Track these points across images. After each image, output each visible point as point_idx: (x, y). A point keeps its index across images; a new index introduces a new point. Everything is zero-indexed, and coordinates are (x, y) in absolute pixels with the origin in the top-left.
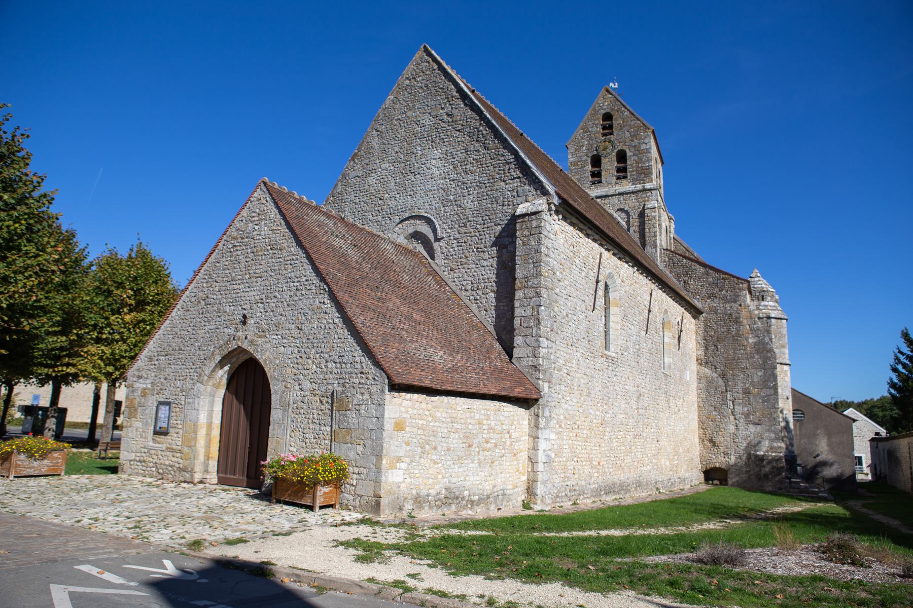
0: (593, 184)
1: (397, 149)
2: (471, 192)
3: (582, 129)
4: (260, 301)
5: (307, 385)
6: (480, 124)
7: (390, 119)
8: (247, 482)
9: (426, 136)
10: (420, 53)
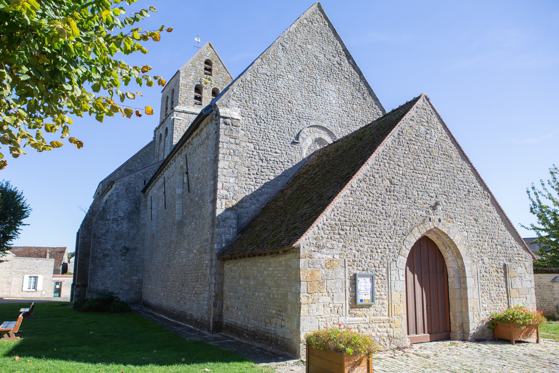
0: (196, 104)
1: (300, 68)
2: (357, 124)
3: (191, 63)
4: (443, 193)
5: (486, 260)
6: (360, 81)
7: (293, 43)
8: (430, 338)
9: (322, 70)
10: (315, 6)
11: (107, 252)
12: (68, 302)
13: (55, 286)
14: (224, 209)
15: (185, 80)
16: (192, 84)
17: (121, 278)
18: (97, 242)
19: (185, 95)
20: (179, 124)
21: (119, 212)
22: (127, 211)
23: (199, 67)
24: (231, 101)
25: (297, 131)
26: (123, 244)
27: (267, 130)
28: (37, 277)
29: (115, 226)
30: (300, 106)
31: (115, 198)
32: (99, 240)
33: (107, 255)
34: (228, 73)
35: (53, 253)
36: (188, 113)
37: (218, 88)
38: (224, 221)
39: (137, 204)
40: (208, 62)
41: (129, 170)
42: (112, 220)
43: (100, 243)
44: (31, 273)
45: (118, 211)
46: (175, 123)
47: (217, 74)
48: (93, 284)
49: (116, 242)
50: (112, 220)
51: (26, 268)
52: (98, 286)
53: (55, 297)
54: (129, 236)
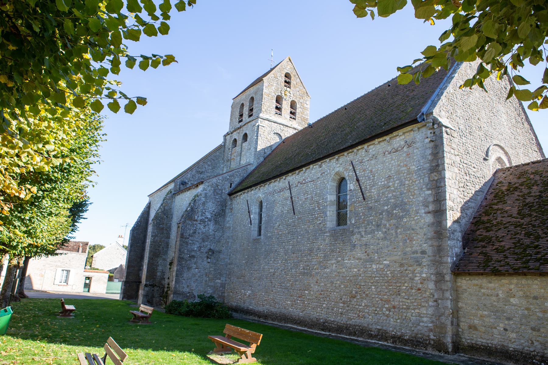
11: (193, 254)
12: (118, 300)
13: (86, 281)
14: (452, 221)
15: (267, 89)
16: (273, 94)
17: (206, 281)
18: (184, 242)
19: (268, 104)
20: (263, 131)
21: (207, 213)
22: (214, 213)
23: (280, 79)
24: (442, 111)
25: (486, 150)
26: (209, 246)
27: (467, 145)
28: (70, 271)
29: (202, 227)
30: (485, 124)
31: (203, 199)
32: (187, 240)
33: (193, 257)
34: (304, 88)
35: (75, 247)
36: (271, 121)
37: (296, 101)
38: (453, 233)
39: (223, 206)
40: (287, 76)
41: (200, 171)
42: (200, 221)
43: (187, 243)
44: (64, 266)
45: (205, 212)
46: (260, 130)
47: (295, 87)
48: (179, 286)
49: (203, 244)
50: (200, 221)
51: (59, 261)
52: (184, 287)
53: (84, 291)
54: (214, 238)
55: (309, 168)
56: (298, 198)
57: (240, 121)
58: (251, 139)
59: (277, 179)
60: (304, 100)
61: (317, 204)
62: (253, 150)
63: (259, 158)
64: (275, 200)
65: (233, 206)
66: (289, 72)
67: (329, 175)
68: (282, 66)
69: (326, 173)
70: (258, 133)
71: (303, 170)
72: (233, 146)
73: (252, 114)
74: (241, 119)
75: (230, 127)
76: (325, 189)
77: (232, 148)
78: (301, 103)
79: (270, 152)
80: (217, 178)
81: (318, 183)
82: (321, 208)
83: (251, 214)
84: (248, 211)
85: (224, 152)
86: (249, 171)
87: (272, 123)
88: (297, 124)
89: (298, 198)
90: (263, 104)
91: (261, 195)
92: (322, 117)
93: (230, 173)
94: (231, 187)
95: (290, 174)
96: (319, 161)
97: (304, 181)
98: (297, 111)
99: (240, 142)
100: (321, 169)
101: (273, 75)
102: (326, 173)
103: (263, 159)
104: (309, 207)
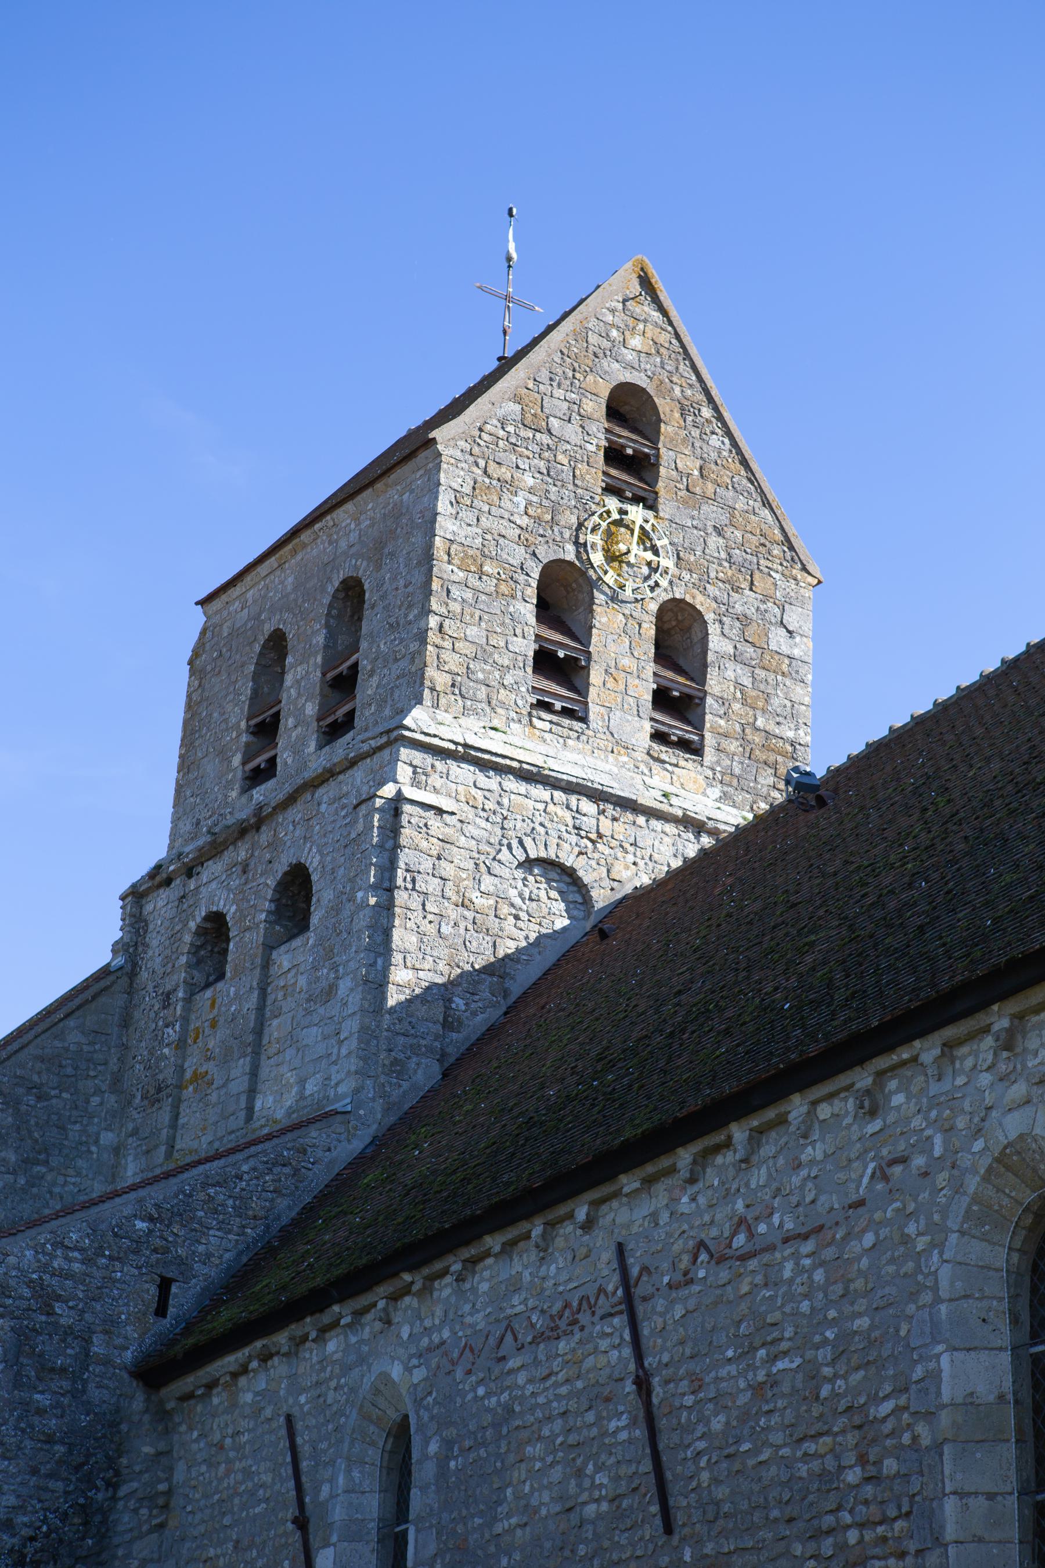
15: (469, 516)
19: (472, 632)
20: (436, 847)
34: (766, 503)
37: (700, 602)
46: (407, 834)
55: (782, 1121)
56: (697, 1385)
57: (258, 776)
58: (336, 910)
59: (523, 1226)
60: (766, 598)
61: (851, 1439)
62: (355, 1001)
63: (397, 1068)
64: (509, 1411)
65: (179, 1475)
66: (639, 379)
67: (942, 1179)
68: (582, 335)
69: (919, 1161)
70: (390, 867)
71: (728, 1144)
72: (199, 977)
73: (351, 715)
74: (261, 760)
75: (176, 820)
76: (913, 1296)
77: (193, 990)
78: (744, 620)
79: (494, 1014)
80: (43, 1236)
81: (855, 1247)
82: (890, 1465)
83: (315, 1542)
84: (292, 1512)
85: (126, 1022)
86: (319, 1177)
87: (511, 784)
88: (715, 792)
89: (697, 1385)
90: (433, 637)
91: (396, 1372)
92: (901, 720)
93: (157, 1193)
94: (161, 1311)
95: (629, 1182)
96: (861, 1062)
97: (740, 1240)
98: (714, 683)
99: (256, 938)
100: (875, 1126)
101: (513, 409)
102: (919, 1161)
103: (436, 1070)
104: (788, 1463)
